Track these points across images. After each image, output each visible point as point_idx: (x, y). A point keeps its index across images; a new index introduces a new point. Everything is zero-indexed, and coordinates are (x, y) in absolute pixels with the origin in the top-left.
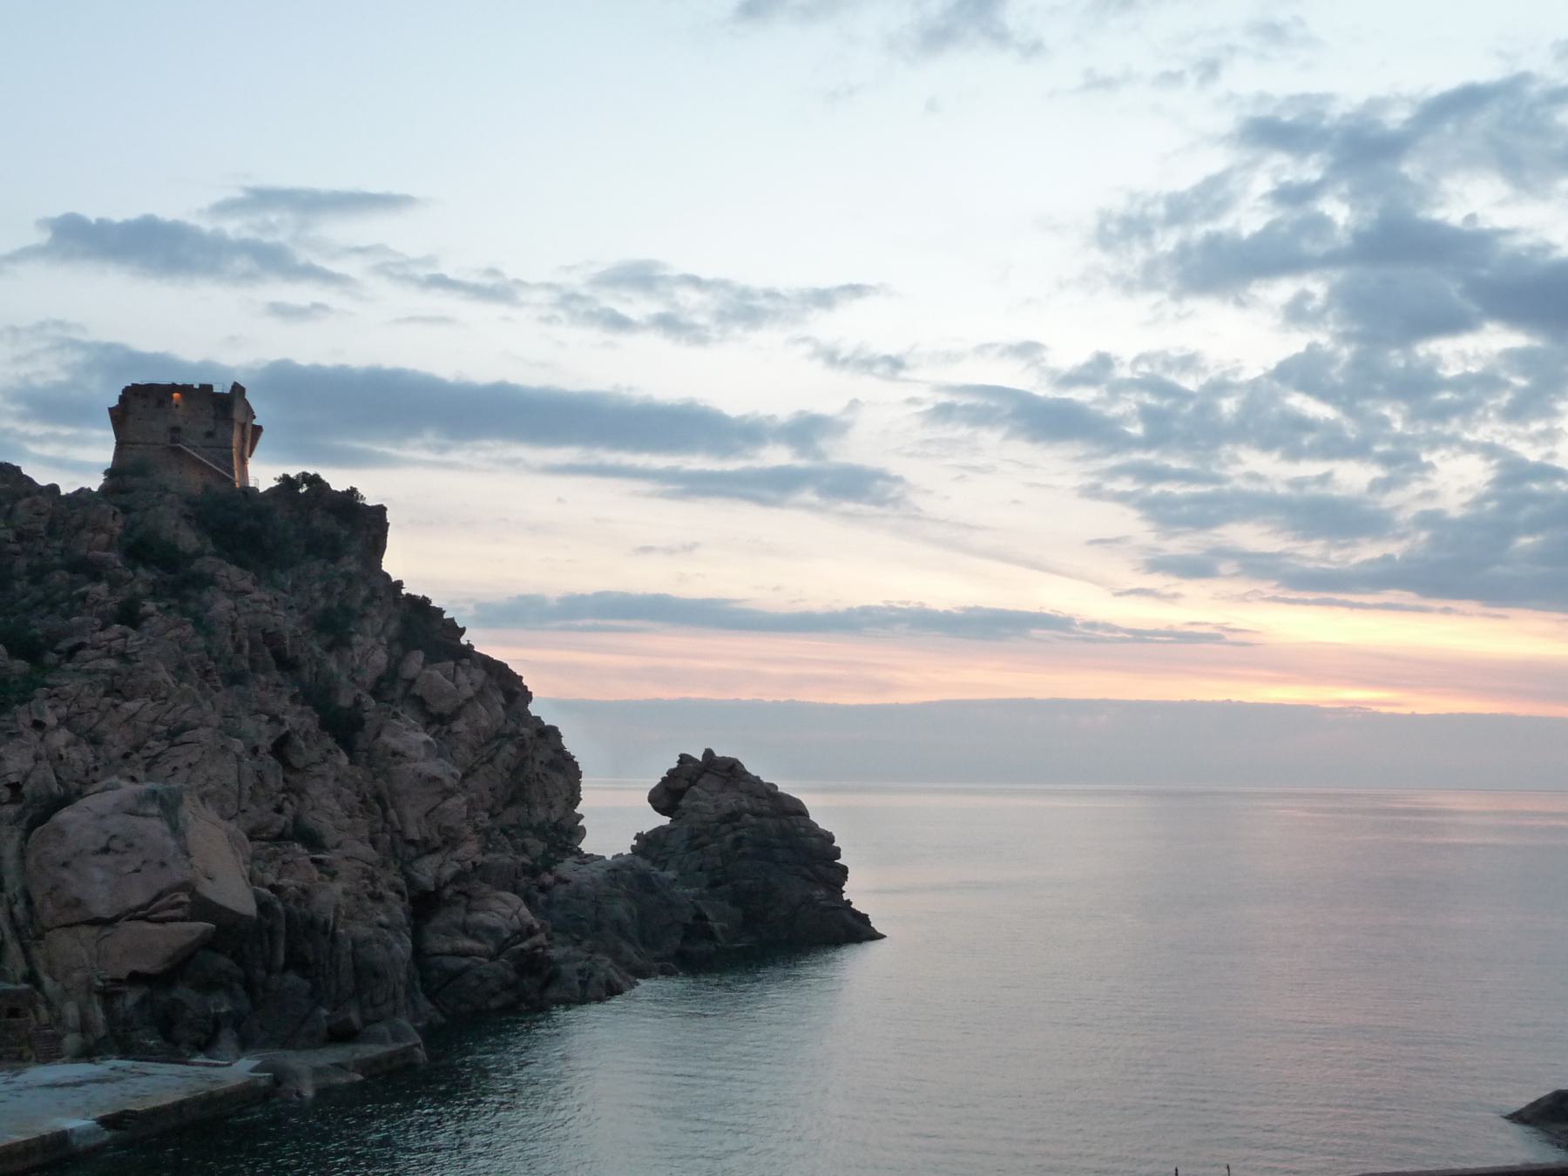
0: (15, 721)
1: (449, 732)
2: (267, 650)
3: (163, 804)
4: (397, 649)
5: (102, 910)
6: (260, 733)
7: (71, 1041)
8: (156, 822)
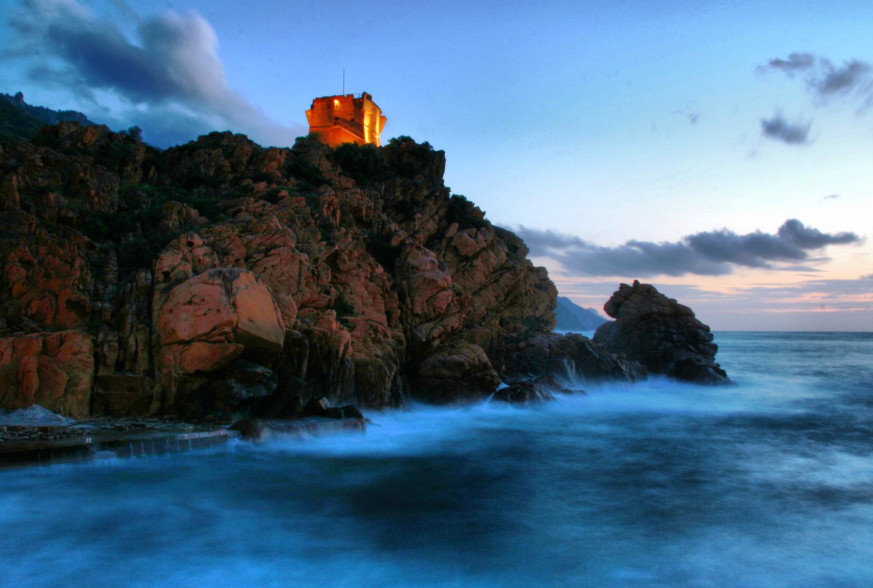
0: (179, 242)
1: (471, 266)
2: (351, 216)
3: (225, 278)
4: (444, 223)
5: (184, 335)
6: (320, 251)
7: (155, 406)
8: (219, 288)
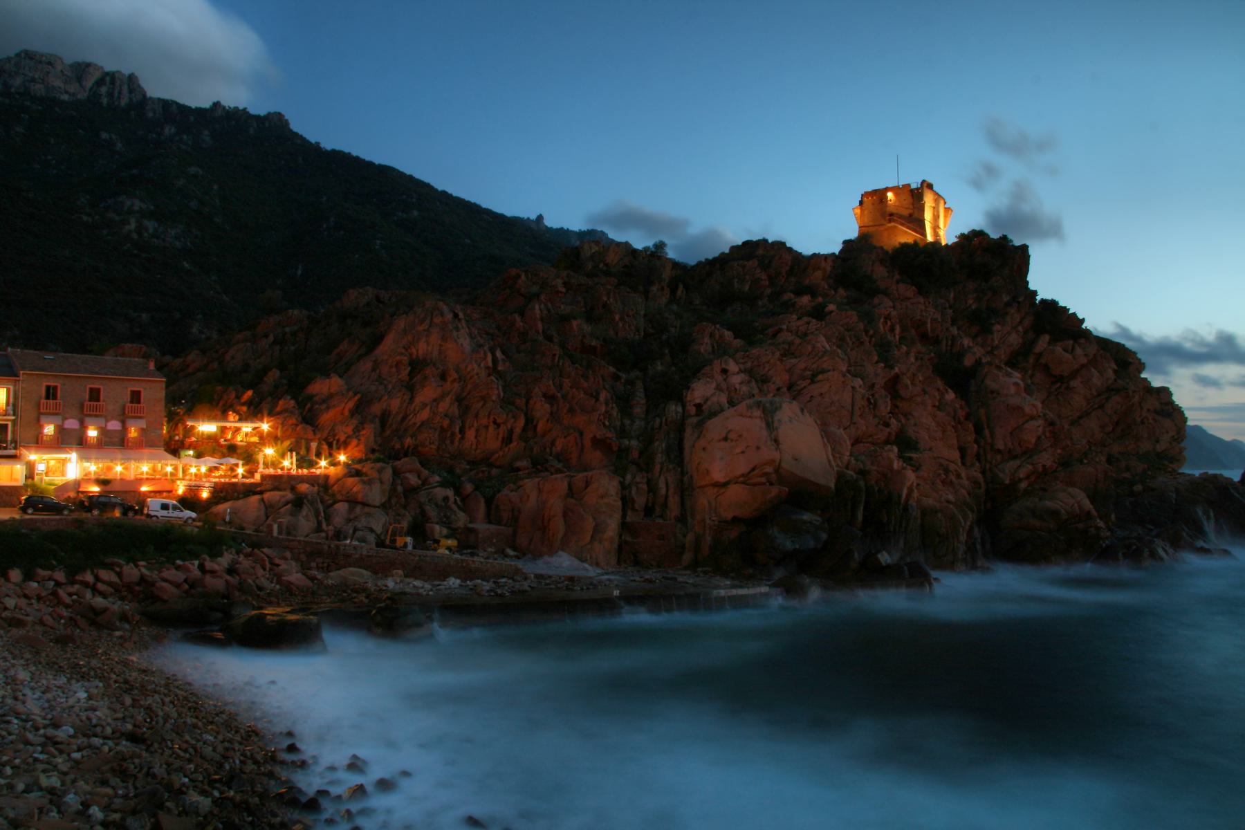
7: (687, 557)
